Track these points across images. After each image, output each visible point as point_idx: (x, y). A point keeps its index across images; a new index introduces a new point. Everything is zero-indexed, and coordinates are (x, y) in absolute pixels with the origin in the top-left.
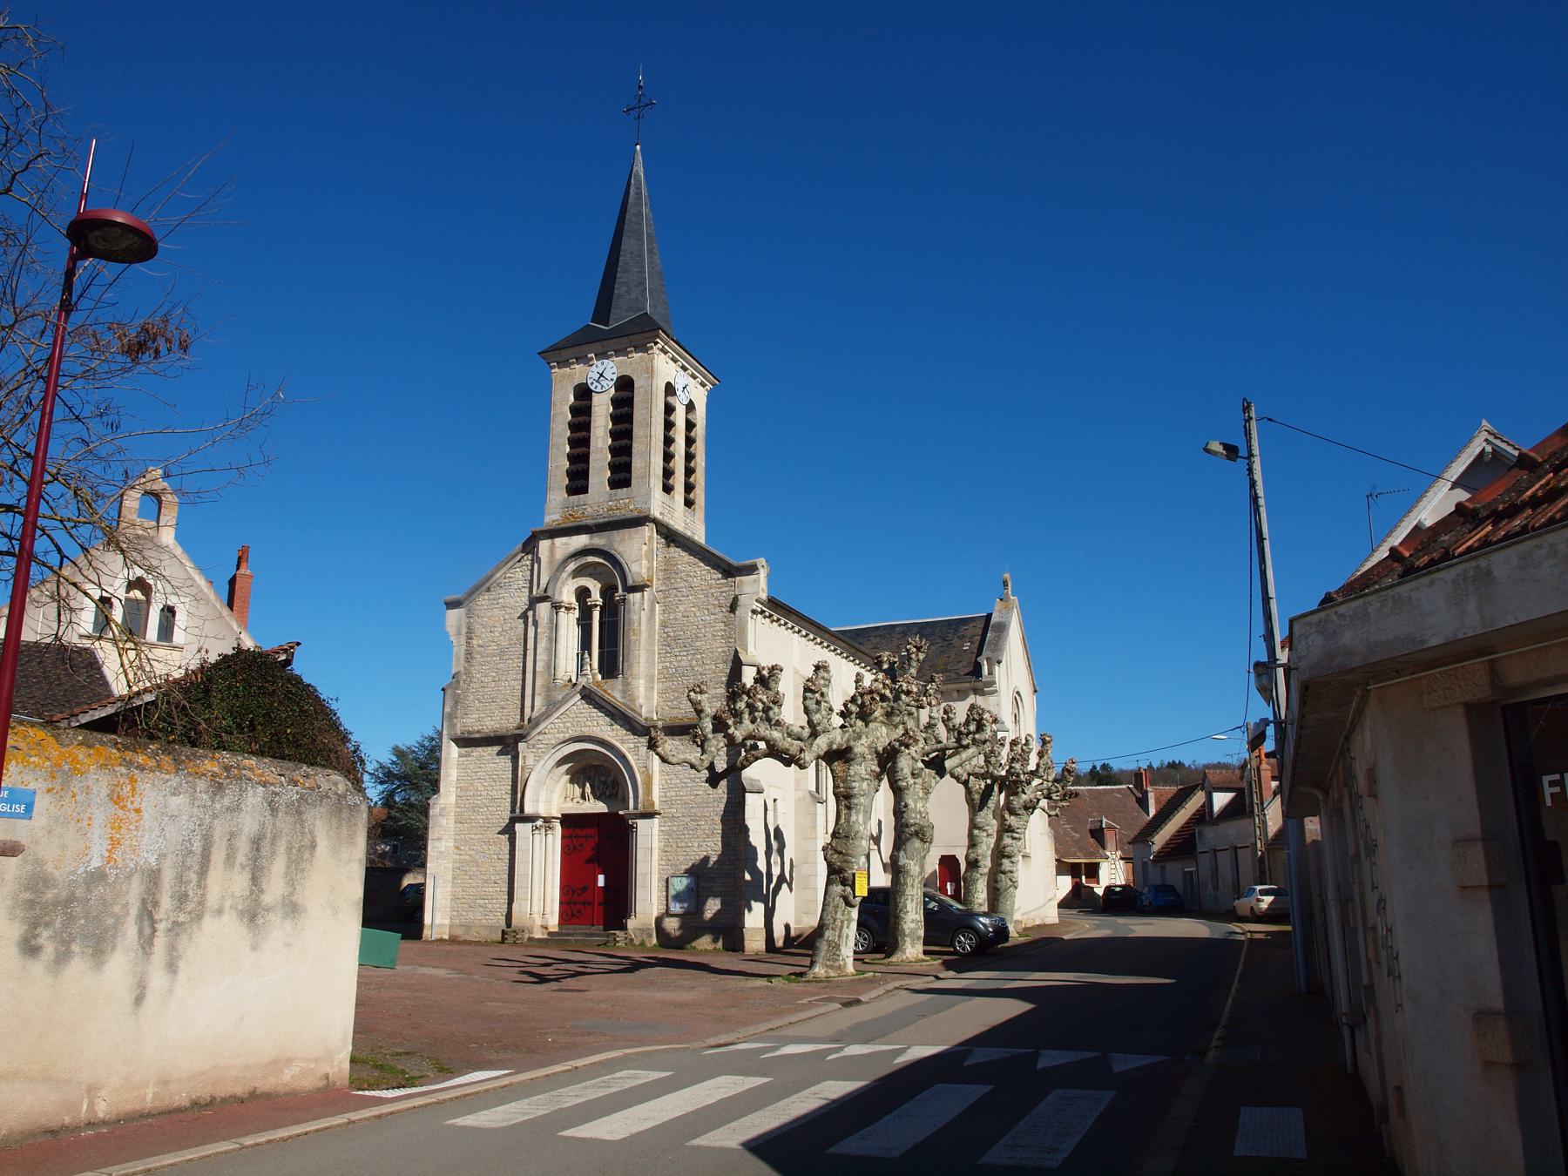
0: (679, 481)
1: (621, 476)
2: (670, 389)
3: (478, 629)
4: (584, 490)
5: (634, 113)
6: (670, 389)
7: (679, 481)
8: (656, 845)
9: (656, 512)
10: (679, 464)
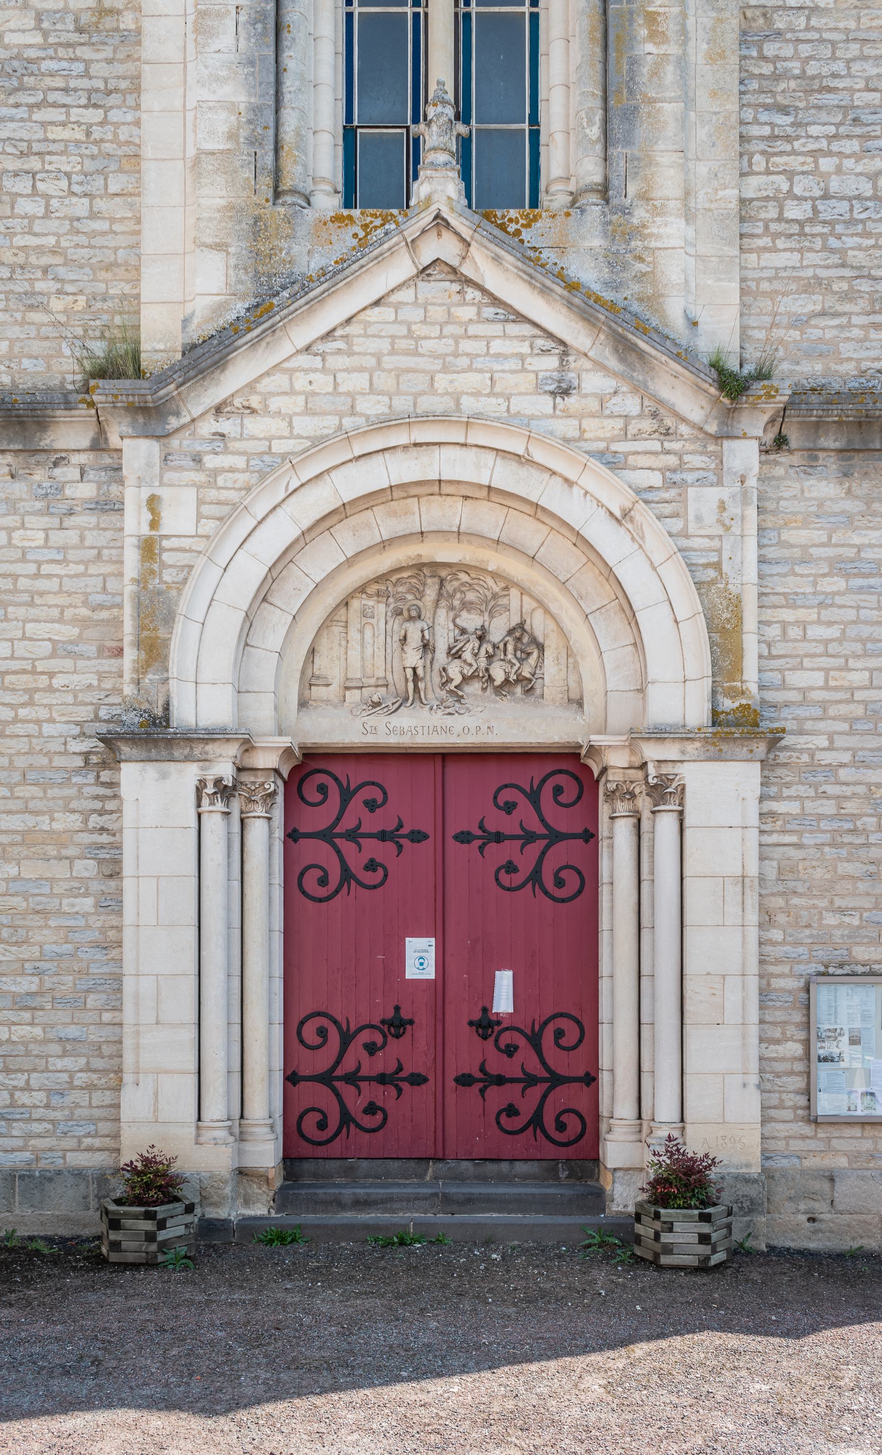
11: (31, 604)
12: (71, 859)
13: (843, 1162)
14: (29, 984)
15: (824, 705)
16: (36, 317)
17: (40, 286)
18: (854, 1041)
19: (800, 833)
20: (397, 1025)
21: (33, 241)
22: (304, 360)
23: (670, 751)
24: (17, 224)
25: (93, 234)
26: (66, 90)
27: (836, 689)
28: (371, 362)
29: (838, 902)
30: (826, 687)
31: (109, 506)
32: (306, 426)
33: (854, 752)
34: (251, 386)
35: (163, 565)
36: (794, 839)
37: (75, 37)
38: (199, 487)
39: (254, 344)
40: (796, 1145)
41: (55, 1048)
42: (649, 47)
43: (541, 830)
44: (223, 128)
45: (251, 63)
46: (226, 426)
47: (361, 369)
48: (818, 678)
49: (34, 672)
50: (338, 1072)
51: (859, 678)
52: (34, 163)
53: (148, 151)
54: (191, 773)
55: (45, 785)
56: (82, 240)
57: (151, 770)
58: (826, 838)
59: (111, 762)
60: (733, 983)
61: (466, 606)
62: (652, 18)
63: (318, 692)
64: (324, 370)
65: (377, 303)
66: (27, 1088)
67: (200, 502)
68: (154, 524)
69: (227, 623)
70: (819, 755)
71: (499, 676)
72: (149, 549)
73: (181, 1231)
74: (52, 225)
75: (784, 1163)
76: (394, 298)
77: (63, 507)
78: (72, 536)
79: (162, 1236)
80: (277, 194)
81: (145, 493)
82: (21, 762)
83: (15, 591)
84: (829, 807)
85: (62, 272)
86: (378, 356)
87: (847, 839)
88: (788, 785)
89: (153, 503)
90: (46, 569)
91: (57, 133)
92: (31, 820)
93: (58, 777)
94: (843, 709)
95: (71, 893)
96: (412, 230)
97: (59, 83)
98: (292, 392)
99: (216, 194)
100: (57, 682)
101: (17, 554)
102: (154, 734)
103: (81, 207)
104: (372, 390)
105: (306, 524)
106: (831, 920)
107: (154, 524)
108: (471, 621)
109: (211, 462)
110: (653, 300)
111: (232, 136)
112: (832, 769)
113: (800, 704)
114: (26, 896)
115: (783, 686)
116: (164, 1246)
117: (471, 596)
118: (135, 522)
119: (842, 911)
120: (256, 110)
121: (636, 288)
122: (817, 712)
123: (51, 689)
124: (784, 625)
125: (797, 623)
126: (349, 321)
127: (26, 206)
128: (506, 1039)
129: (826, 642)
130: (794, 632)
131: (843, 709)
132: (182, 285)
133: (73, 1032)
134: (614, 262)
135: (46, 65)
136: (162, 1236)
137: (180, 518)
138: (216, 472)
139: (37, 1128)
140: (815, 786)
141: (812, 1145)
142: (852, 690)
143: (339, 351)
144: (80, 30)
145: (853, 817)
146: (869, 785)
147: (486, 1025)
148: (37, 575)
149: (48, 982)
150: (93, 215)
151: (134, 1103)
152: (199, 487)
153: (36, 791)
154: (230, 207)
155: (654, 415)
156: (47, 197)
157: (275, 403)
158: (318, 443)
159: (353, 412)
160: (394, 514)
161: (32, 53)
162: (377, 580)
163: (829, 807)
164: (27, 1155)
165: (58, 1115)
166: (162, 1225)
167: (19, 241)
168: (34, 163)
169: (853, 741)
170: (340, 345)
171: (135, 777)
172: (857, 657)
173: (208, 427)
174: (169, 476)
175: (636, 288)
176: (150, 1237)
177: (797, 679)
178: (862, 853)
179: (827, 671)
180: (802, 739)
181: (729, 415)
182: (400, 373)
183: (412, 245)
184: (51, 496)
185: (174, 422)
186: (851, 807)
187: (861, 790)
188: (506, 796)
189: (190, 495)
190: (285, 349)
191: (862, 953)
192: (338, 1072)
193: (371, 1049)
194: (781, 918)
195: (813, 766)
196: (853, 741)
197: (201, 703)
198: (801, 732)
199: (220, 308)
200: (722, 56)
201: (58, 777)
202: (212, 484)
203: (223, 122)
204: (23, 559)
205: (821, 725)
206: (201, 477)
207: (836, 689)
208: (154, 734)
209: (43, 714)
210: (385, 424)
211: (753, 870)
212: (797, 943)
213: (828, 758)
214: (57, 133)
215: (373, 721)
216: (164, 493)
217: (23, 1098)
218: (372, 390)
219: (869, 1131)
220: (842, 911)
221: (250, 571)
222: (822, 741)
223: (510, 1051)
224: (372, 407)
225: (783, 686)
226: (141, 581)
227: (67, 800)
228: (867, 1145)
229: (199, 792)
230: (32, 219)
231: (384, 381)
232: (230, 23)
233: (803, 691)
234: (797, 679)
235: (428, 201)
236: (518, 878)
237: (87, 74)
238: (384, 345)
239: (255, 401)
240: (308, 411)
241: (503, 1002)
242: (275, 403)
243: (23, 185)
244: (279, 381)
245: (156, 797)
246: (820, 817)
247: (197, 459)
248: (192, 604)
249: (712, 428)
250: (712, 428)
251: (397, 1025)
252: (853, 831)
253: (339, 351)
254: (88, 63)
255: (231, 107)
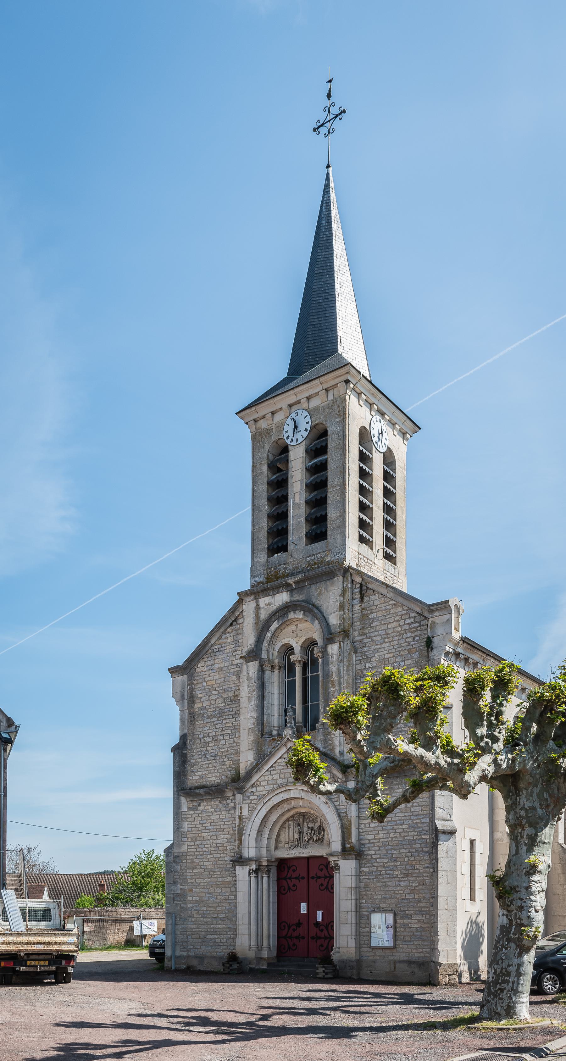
0: (377, 470)
1: (318, 529)
2: (364, 435)
3: (199, 694)
4: (284, 548)
5: (323, 130)
6: (364, 435)
7: (377, 470)
8: (276, 702)
9: (351, 561)
10: (369, 1004)
11: (223, 831)
12: (230, 887)
13: (378, 958)
14: (223, 915)
15: (374, 843)
16: (224, 767)
17: (225, 760)
18: (379, 928)
19: (369, 876)
20: (299, 924)
21: (223, 750)
22: (267, 773)
23: (336, 859)
24: (221, 746)
25: (234, 747)
26: (228, 715)
27: (377, 839)
28: (279, 771)
29: (377, 893)
30: (374, 839)
31: (235, 808)
32: (268, 788)
33: (380, 855)
34: (258, 780)
35: (243, 822)
36: (367, 877)
37: (230, 703)
38: (249, 804)
39: (256, 772)
40: (368, 954)
41: (227, 930)
42: (332, 689)
43: (328, 875)
44: (252, 722)
45: (257, 707)
46: (254, 790)
47: (277, 774)
48: (372, 837)
49: (224, 846)
50: (328, 939)
51: (381, 836)
52: (223, 732)
53: (241, 728)
54: (247, 868)
55: (226, 871)
56: (232, 748)
57: (241, 868)
58: (374, 877)
59: (234, 867)
60: (349, 913)
61: (310, 821)
62: (332, 681)
63: (280, 845)
64: (271, 775)
65: (280, 758)
66: (223, 938)
67: (249, 807)
68: (241, 813)
69: (254, 834)
70: (373, 856)
71: (315, 839)
72: (240, 818)
73: (236, 967)
74: (227, 746)
75: (365, 958)
76: (284, 756)
77: (228, 809)
78: (230, 815)
79: (231, 968)
80: (263, 735)
81: (240, 806)
82: (222, 866)
83: (221, 828)
84: (375, 869)
85: (228, 756)
86: (281, 770)
87: (379, 877)
88: (366, 864)
89: (241, 808)
90: (226, 823)
91: (227, 725)
92: (223, 879)
93: (228, 869)
94: (378, 844)
95: (230, 895)
96: (284, 742)
97: (227, 714)
98: (265, 780)
99: (251, 738)
100: (228, 848)
101: (220, 820)
102: (240, 860)
103: (231, 741)
104: (280, 778)
105: (268, 810)
106: (375, 897)
107: (241, 813)
108: (311, 825)
109: (251, 798)
110: (333, 750)
111: (254, 724)
112: (376, 859)
113: (368, 843)
114: (223, 896)
115: (365, 839)
116: (231, 970)
117: (311, 819)
118: (238, 813)
119: (378, 895)
120: (258, 717)
121: (329, 747)
122: (372, 845)
123: (227, 850)
124: (365, 824)
125: (368, 823)
126: (275, 763)
127: (223, 742)
128: (321, 927)
129: (374, 827)
130: (367, 826)
131: (378, 844)
132: (247, 758)
133: (231, 926)
134: (325, 741)
135: (226, 710)
136: (231, 968)
137: (246, 812)
138: (252, 800)
139: (225, 947)
140: (372, 864)
141: (371, 954)
142: (380, 839)
143: (273, 770)
144: (231, 701)
145: (381, 871)
146: (383, 863)
147: (317, 924)
148: (224, 825)
149: (227, 915)
150: (234, 742)
151: (238, 941)
152: (249, 804)
153: (224, 872)
154: (254, 740)
155: (333, 777)
156: (226, 740)
157: (262, 783)
158: (269, 792)
159: (276, 783)
160: (288, 804)
161: (223, 708)
162: (291, 817)
163: (375, 869)
164: (223, 953)
165: (228, 944)
166: (231, 965)
167: (221, 750)
168: (223, 732)
169: (380, 852)
170: (274, 768)
171: (238, 869)
172: (381, 831)
173: (250, 790)
174: (244, 802)
175: (329, 747)
176: (229, 968)
177: (368, 837)
178: (382, 880)
179: (374, 835)
180: (369, 852)
181: (346, 777)
182: (284, 773)
183: (285, 745)
184: (227, 806)
185: (244, 790)
186: (379, 869)
187: (382, 864)
188: (321, 867)
189: (247, 806)
190: (264, 771)
191: (382, 905)
192: (328, 939)
193: (294, 930)
194: (365, 897)
195: (371, 859)
196: (380, 852)
197: (249, 852)
198: (369, 850)
199: (252, 763)
200: (349, 686)
201: (228, 869)
202: (251, 803)
203: (252, 721)
204: (222, 821)
205: (373, 848)
206: (248, 801)
207: (377, 839)
208: (240, 860)
209: (225, 855)
210: (280, 787)
211: (354, 886)
212: (368, 903)
213: (374, 857)
214: (227, 725)
215: (289, 852)
216: (243, 806)
217: (222, 941)
218: (280, 778)
219: (384, 951)
220: (378, 895)
221: (258, 821)
222: (373, 852)
223: (322, 930)
224: (279, 782)
225: (365, 839)
226: (239, 826)
227: (230, 874)
228: (383, 954)
229: (250, 871)
230: (223, 745)
231: (282, 776)
232: (254, 698)
233: (369, 840)
234: (368, 837)
235: (286, 736)
236: (323, 888)
237: (232, 711)
238: (281, 767)
239: (258, 783)
240: (268, 784)
241: (319, 918)
242: (262, 783)
243: (221, 738)
244: (263, 778)
245: (242, 873)
246: (373, 872)
247: (249, 798)
248: (247, 830)
249: (344, 780)
250: (344, 780)
251: (299, 924)
252: (380, 875)
253: (273, 770)
254: (232, 708)
255: (254, 717)
